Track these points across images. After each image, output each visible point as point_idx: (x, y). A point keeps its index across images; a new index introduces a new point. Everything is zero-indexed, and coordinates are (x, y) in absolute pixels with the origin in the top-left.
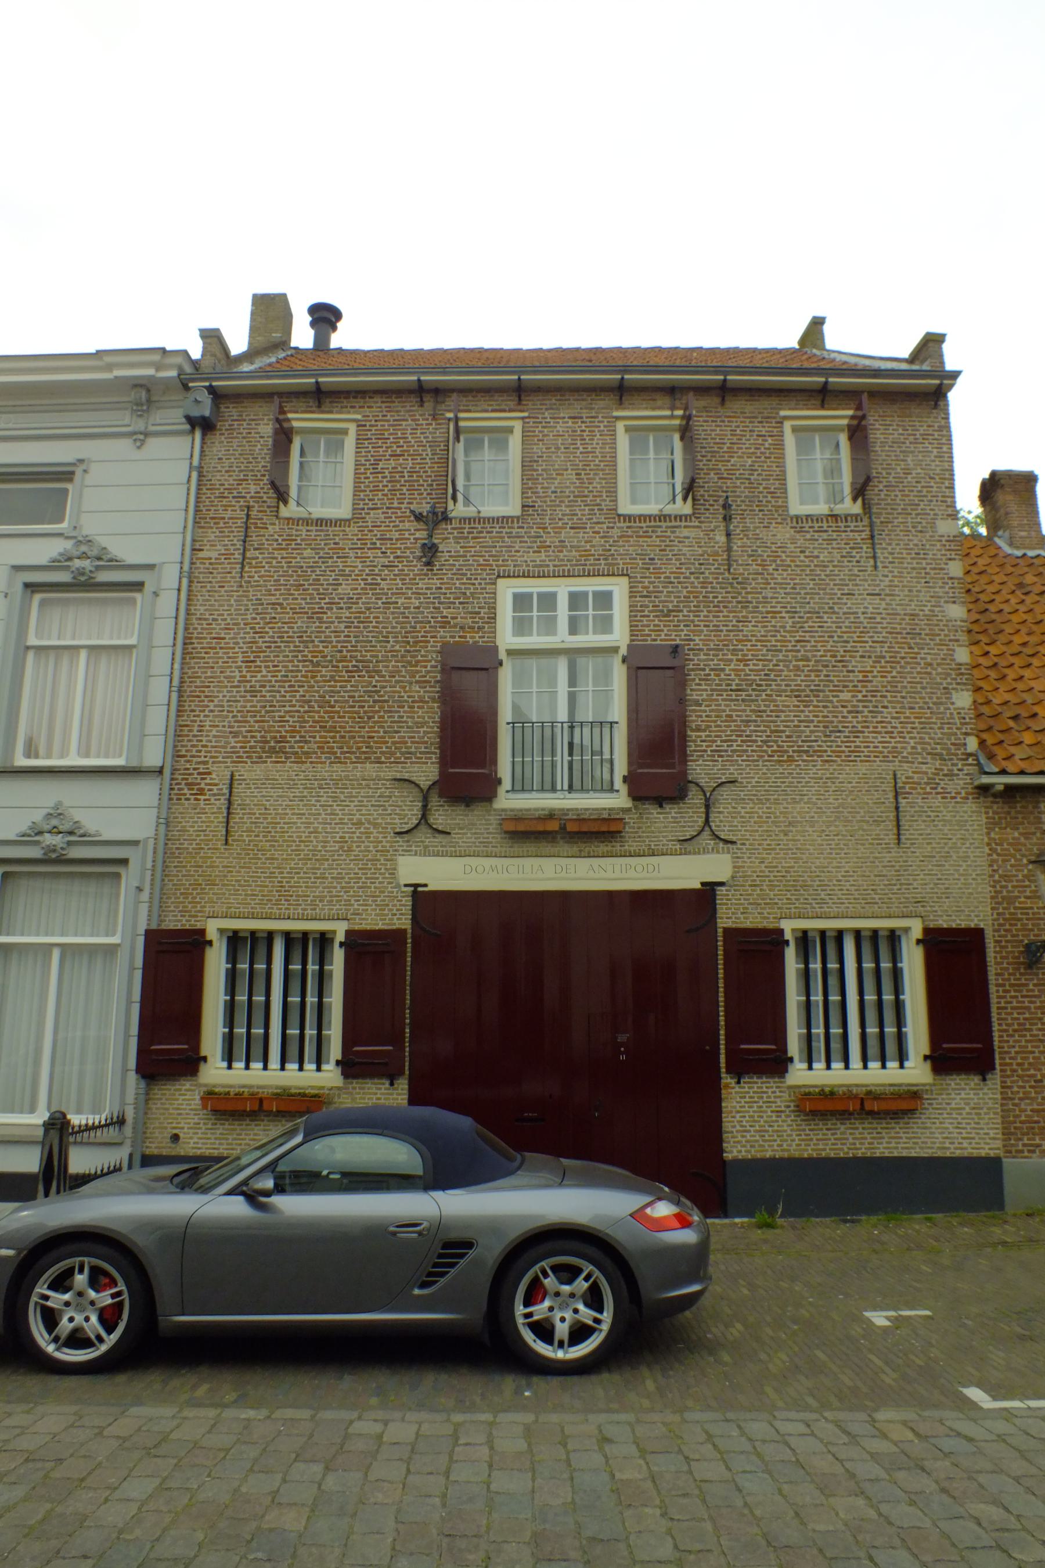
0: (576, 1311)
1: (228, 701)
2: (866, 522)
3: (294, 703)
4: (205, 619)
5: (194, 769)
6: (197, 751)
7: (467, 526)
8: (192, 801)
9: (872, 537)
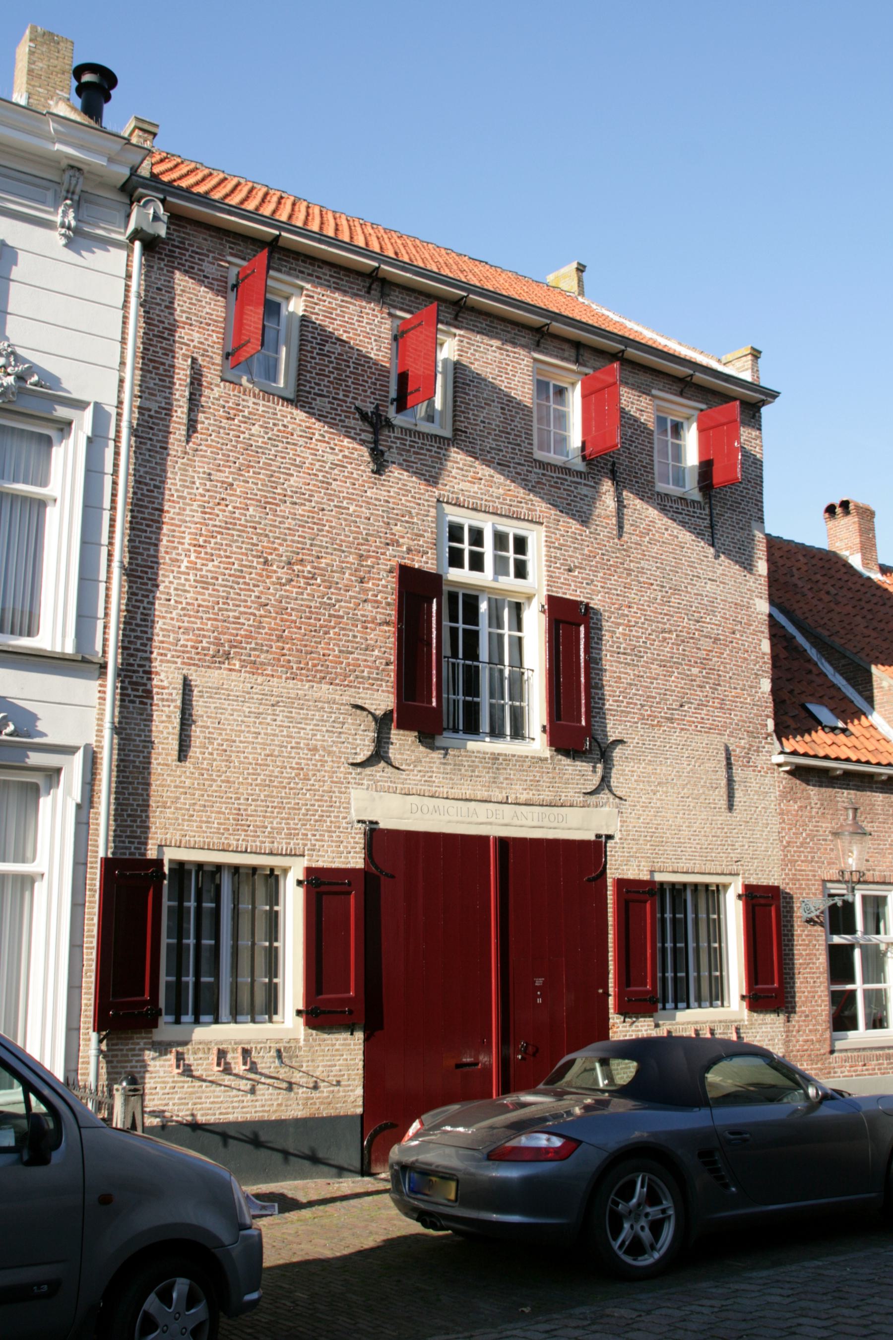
0: (647, 1215)
1: (176, 589)
2: (707, 511)
3: (249, 604)
4: (146, 484)
5: (140, 666)
6: (142, 644)
7: (408, 438)
8: (137, 705)
9: (712, 526)
